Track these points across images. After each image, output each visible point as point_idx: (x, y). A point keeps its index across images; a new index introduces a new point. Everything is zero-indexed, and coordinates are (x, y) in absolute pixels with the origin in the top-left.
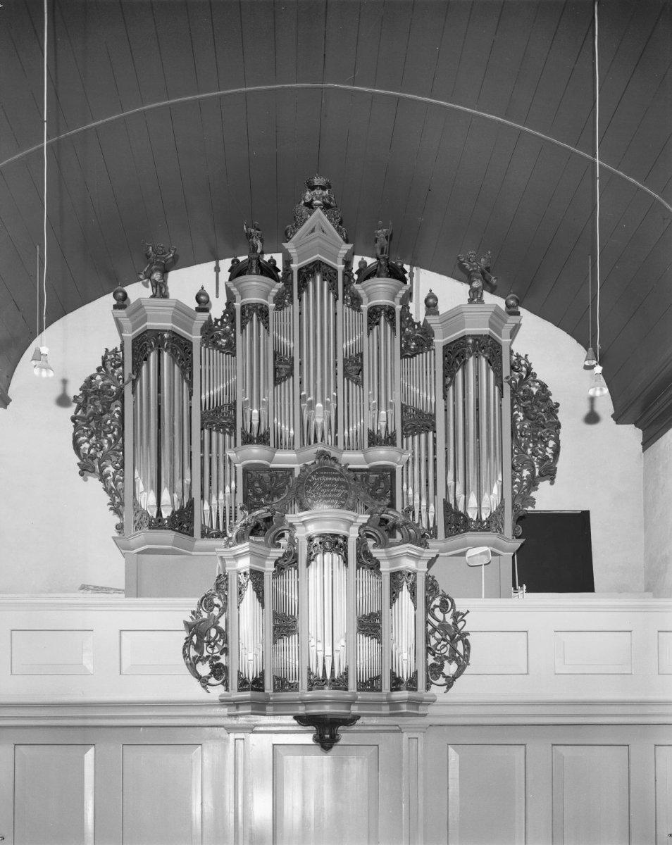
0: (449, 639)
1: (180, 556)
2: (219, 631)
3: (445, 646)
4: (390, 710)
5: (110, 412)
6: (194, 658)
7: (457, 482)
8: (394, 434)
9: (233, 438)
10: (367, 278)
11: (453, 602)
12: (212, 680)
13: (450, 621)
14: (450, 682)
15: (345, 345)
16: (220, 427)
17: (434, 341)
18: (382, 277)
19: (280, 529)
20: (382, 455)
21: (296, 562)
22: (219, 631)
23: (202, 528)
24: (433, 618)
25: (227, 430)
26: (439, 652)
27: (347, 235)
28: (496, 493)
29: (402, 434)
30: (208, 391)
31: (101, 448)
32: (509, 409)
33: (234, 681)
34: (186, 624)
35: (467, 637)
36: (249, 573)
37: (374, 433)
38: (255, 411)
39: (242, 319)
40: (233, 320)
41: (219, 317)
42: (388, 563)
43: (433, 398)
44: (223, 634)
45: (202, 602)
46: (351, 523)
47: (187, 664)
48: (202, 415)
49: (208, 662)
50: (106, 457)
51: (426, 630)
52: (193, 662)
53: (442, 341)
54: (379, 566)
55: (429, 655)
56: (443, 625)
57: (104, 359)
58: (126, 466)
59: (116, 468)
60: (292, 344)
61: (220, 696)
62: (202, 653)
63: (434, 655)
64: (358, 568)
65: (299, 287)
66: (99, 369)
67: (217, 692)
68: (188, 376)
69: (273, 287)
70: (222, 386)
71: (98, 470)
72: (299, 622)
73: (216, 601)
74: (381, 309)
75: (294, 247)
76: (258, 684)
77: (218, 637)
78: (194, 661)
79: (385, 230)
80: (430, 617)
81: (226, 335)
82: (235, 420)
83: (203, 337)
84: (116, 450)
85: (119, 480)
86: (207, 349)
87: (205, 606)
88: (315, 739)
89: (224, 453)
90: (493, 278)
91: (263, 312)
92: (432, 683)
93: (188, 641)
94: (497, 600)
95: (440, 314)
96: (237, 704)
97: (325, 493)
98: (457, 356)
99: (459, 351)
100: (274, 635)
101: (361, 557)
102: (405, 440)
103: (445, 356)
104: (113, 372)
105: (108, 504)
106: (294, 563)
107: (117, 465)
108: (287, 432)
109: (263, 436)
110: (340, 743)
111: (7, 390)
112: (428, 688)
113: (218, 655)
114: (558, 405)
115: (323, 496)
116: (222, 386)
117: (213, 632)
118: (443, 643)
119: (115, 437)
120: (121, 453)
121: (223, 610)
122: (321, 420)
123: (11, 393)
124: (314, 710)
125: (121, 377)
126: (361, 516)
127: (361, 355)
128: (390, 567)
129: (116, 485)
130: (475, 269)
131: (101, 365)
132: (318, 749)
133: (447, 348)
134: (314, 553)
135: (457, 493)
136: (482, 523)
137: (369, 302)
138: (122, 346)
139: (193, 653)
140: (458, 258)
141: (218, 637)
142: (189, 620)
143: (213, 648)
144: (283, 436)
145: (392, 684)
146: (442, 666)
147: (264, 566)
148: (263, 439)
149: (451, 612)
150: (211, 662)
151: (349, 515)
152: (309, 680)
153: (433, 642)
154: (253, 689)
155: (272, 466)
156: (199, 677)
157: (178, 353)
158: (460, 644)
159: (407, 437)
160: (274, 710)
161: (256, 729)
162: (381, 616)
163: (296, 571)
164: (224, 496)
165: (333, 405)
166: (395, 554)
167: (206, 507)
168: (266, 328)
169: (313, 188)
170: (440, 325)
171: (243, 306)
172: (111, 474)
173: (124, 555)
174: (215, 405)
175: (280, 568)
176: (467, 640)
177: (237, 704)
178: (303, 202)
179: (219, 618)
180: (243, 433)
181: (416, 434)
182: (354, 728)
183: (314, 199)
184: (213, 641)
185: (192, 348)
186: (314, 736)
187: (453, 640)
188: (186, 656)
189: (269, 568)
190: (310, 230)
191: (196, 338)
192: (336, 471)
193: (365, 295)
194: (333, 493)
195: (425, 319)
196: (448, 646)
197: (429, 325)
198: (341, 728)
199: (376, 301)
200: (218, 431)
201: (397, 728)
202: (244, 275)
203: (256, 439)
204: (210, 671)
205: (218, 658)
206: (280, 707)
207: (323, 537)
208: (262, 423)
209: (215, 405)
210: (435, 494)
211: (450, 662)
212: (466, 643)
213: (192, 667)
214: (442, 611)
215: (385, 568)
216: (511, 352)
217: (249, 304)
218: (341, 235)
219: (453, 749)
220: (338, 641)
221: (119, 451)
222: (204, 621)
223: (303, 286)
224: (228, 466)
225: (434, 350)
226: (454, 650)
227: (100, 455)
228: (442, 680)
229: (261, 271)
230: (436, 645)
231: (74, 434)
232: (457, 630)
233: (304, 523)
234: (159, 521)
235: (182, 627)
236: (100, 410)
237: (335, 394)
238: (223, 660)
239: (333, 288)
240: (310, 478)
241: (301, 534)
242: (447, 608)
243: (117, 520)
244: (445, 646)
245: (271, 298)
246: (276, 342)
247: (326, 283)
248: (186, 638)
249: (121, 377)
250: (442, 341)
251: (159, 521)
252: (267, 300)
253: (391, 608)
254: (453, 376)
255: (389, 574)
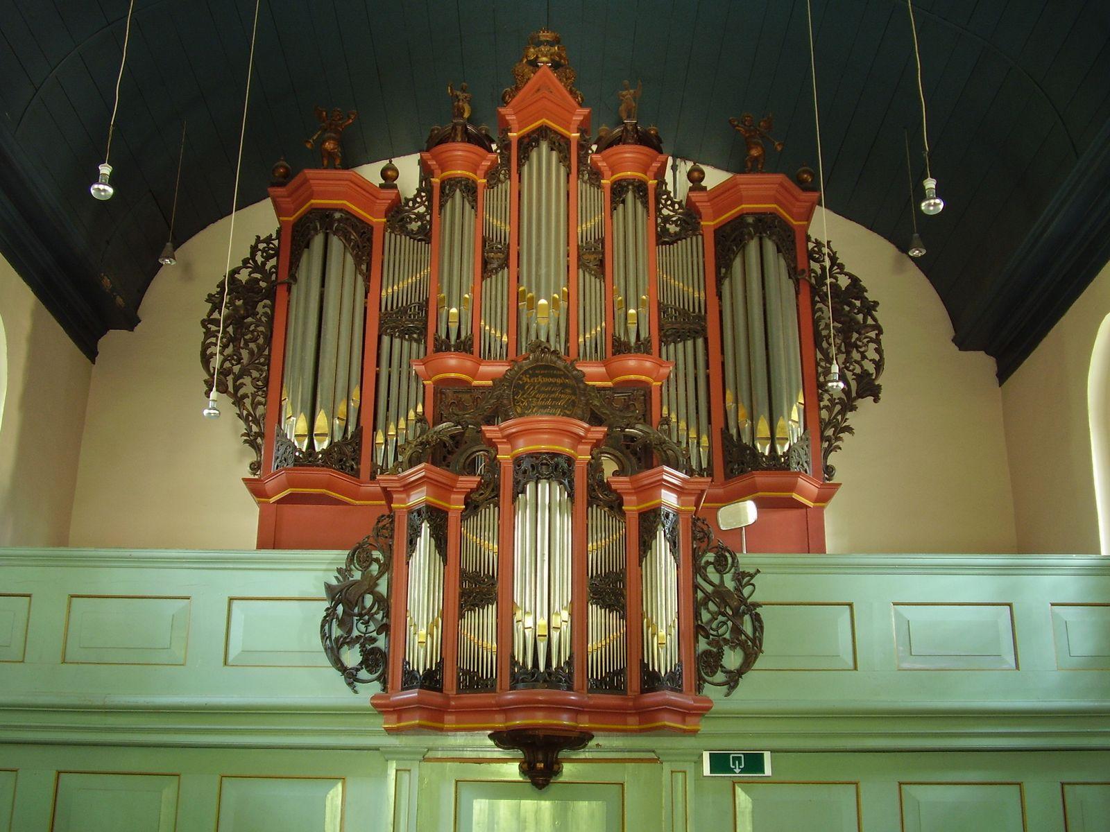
0: (731, 613)
1: (344, 507)
2: (378, 599)
3: (724, 623)
4: (640, 724)
5: (254, 314)
6: (337, 639)
7: (740, 405)
8: (648, 341)
9: (422, 347)
10: (610, 145)
11: (734, 558)
12: (363, 674)
13: (730, 584)
14: (733, 680)
15: (579, 229)
16: (405, 333)
17: (702, 223)
18: (629, 143)
19: (474, 450)
20: (635, 366)
21: (498, 496)
22: (378, 599)
23: (372, 468)
24: (705, 580)
25: (415, 336)
26: (715, 633)
27: (582, 98)
28: (797, 419)
29: (661, 341)
30: (395, 288)
31: (239, 361)
32: (809, 310)
33: (397, 677)
34: (328, 587)
35: (758, 610)
36: (424, 510)
37: (620, 339)
38: (454, 310)
39: (441, 197)
40: (430, 199)
41: (411, 196)
42: (634, 498)
43: (702, 294)
44: (383, 603)
45: (353, 555)
46: (579, 439)
47: (326, 649)
48: (380, 317)
49: (358, 646)
50: (244, 372)
51: (695, 598)
52: (335, 647)
53: (712, 223)
54: (621, 504)
55: (700, 637)
56: (720, 594)
57: (254, 249)
58: (270, 385)
59: (258, 388)
60: (508, 227)
61: (372, 698)
62: (350, 631)
63: (707, 637)
64: (590, 504)
65: (519, 160)
66: (245, 262)
67: (369, 690)
68: (364, 267)
69: (484, 159)
70: (410, 281)
71: (231, 389)
72: (499, 586)
73: (376, 554)
74: (628, 184)
75: (513, 113)
76: (431, 680)
77: (376, 606)
78: (337, 644)
79: (632, 91)
80: (700, 580)
81: (420, 217)
82: (426, 323)
83: (388, 221)
84: (259, 363)
85: (260, 403)
86: (393, 235)
87: (359, 561)
88: (523, 771)
89: (410, 366)
90: (777, 143)
91: (470, 190)
92: (705, 681)
93: (330, 613)
94: (802, 555)
95: (708, 189)
96: (399, 710)
97: (542, 400)
98: (734, 240)
99: (737, 233)
100: (461, 607)
101: (594, 490)
102: (664, 349)
103: (717, 243)
104: (264, 264)
105: (242, 435)
106: (493, 497)
107: (260, 383)
108: (498, 340)
109: (464, 343)
110: (561, 779)
111: (137, 307)
112: (699, 689)
113: (374, 634)
114: (876, 303)
115: (539, 403)
116: (410, 281)
117: (369, 600)
118: (721, 618)
119: (258, 346)
120: (266, 368)
121: (386, 567)
122: (546, 321)
123: (140, 313)
124: (518, 722)
125: (273, 270)
126: (593, 429)
127: (603, 241)
128: (638, 504)
129: (254, 409)
130: (753, 134)
131: (249, 256)
132: (529, 787)
133: (720, 233)
134: (522, 482)
135: (741, 419)
136: (779, 458)
137: (612, 175)
138: (279, 232)
139: (336, 632)
140: (730, 121)
141: (376, 606)
142: (334, 582)
143: (366, 623)
144: (492, 349)
145: (643, 682)
146: (720, 655)
147: (448, 501)
148: (464, 346)
149: (733, 570)
150: (363, 646)
151: (580, 427)
152: (513, 674)
153: (706, 616)
154: (422, 687)
155: (476, 383)
156: (342, 669)
157: (352, 237)
158: (747, 618)
159: (667, 345)
160: (457, 723)
161: (430, 754)
162: (625, 576)
163: (496, 509)
164: (407, 424)
165: (563, 304)
166: (646, 482)
167: (380, 438)
168: (473, 208)
169: (539, 43)
170: (709, 204)
171: (443, 182)
172: (250, 395)
173: (259, 503)
174: (400, 305)
175: (472, 507)
176: (757, 615)
177: (399, 710)
178: (525, 60)
179: (378, 579)
180: (436, 339)
181: (681, 341)
182: (582, 755)
183: (540, 56)
184: (368, 613)
185: (372, 234)
186: (520, 767)
187: (738, 615)
188: (325, 636)
189: (456, 505)
190: (536, 88)
191: (378, 221)
192: (559, 369)
193: (607, 168)
194: (553, 399)
195: (688, 196)
196: (730, 623)
197: (695, 203)
198: (563, 754)
199: (619, 175)
200: (402, 338)
201: (652, 755)
202: (447, 143)
203: (454, 346)
204: (360, 659)
205: (374, 640)
206: (470, 717)
207: (537, 459)
208: (463, 327)
209: (400, 305)
210: (709, 422)
211: (733, 648)
212: (757, 619)
213: (334, 651)
214: (718, 571)
215: (631, 507)
216: (808, 238)
217: (449, 179)
218: (575, 97)
219: (746, 792)
220: (558, 614)
221: (263, 364)
222: (356, 582)
223: (524, 155)
224: (413, 384)
225: (702, 235)
226: (737, 630)
227: (236, 369)
228: (720, 677)
229: (468, 138)
230: (711, 621)
231: (203, 343)
232: (743, 600)
233: (510, 438)
234: (310, 455)
235: (323, 594)
236: (242, 312)
237: (565, 289)
238: (381, 643)
239: (565, 159)
240: (520, 379)
241: (504, 456)
242: (727, 565)
243: (252, 456)
244: (724, 623)
245: (481, 172)
246: (485, 225)
247: (554, 154)
248: (327, 609)
249: (273, 270)
250: (712, 223)
251: (310, 455)
252: (476, 174)
253: (641, 566)
254: (729, 266)
255: (637, 516)
